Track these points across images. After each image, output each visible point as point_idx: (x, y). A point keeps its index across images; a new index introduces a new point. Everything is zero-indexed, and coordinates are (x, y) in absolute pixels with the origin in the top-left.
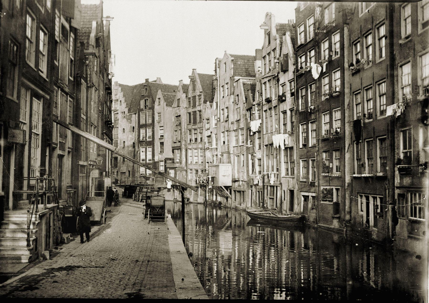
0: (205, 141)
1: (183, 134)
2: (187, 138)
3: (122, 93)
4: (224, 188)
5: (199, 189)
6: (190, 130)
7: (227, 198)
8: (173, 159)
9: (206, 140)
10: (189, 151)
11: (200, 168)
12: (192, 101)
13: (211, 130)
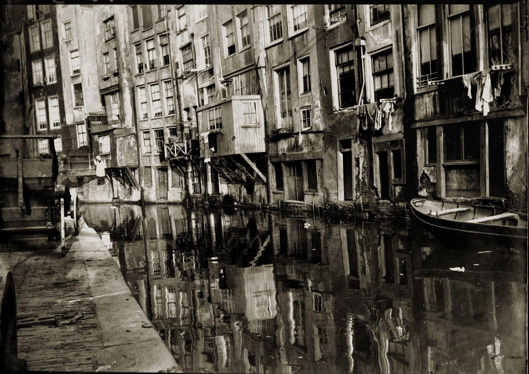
0: (177, 60)
1: (123, 54)
2: (133, 64)
4: (246, 158)
5: (170, 171)
6: (138, 45)
7: (250, 186)
8: (106, 117)
9: (178, 57)
10: (140, 94)
11: (166, 125)
13: (190, 30)
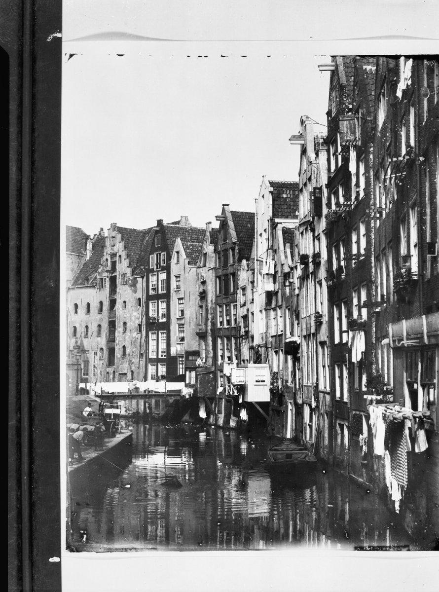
3: (122, 244)
12: (222, 255)
